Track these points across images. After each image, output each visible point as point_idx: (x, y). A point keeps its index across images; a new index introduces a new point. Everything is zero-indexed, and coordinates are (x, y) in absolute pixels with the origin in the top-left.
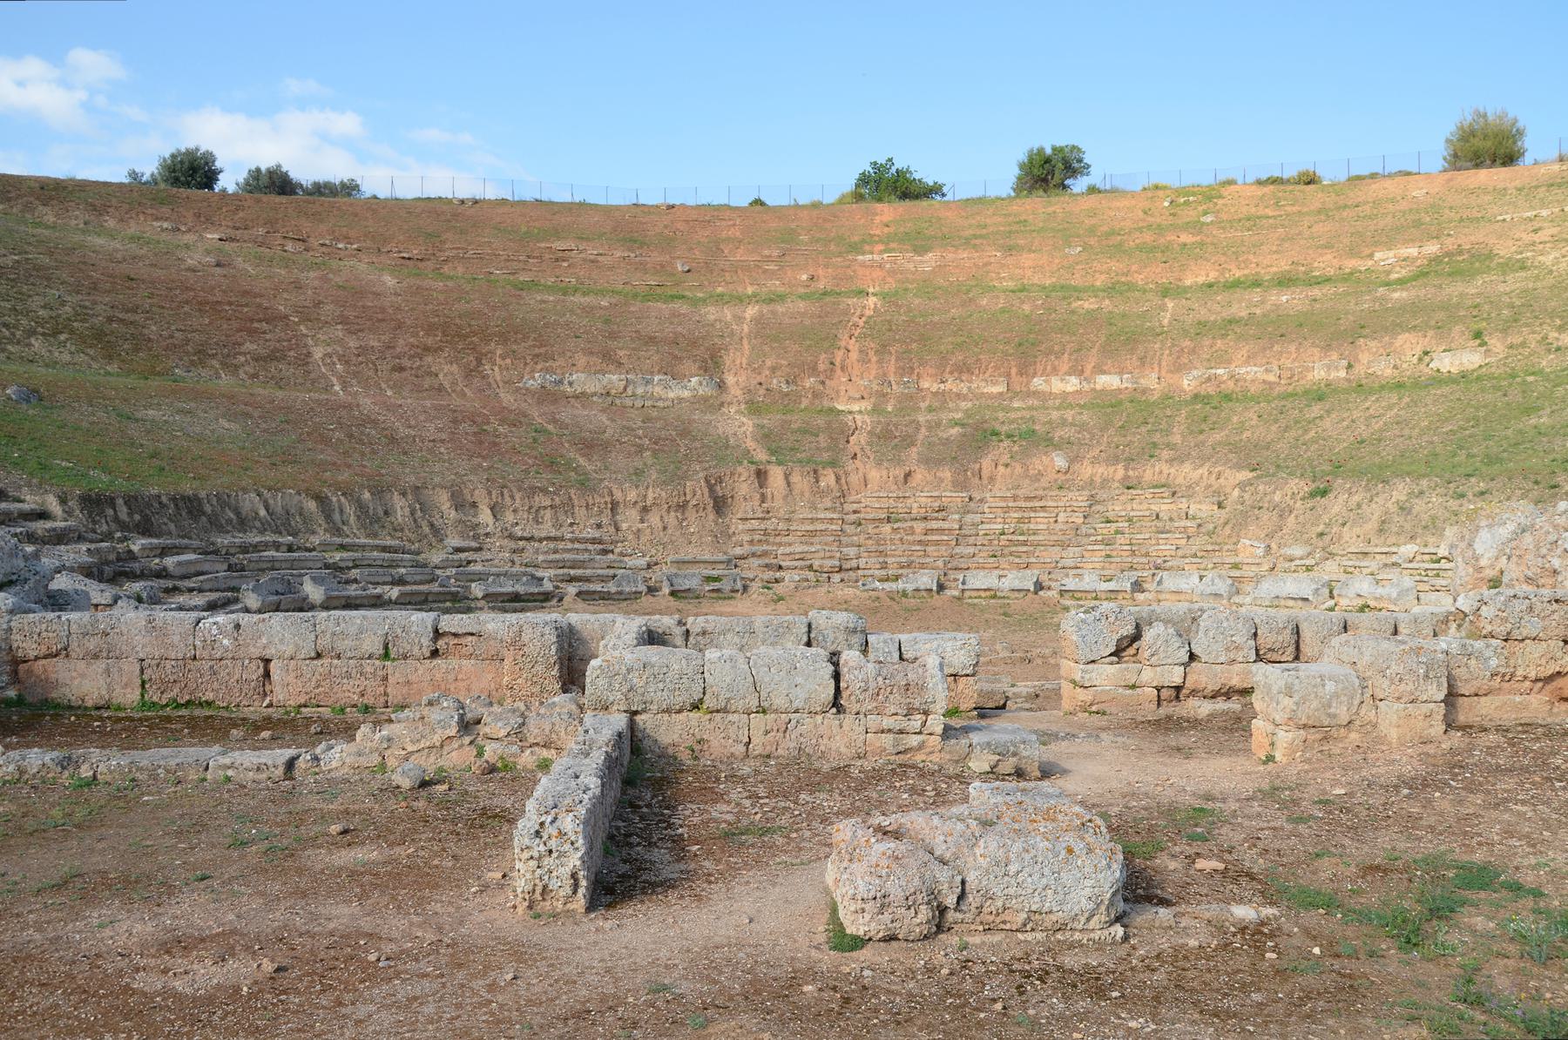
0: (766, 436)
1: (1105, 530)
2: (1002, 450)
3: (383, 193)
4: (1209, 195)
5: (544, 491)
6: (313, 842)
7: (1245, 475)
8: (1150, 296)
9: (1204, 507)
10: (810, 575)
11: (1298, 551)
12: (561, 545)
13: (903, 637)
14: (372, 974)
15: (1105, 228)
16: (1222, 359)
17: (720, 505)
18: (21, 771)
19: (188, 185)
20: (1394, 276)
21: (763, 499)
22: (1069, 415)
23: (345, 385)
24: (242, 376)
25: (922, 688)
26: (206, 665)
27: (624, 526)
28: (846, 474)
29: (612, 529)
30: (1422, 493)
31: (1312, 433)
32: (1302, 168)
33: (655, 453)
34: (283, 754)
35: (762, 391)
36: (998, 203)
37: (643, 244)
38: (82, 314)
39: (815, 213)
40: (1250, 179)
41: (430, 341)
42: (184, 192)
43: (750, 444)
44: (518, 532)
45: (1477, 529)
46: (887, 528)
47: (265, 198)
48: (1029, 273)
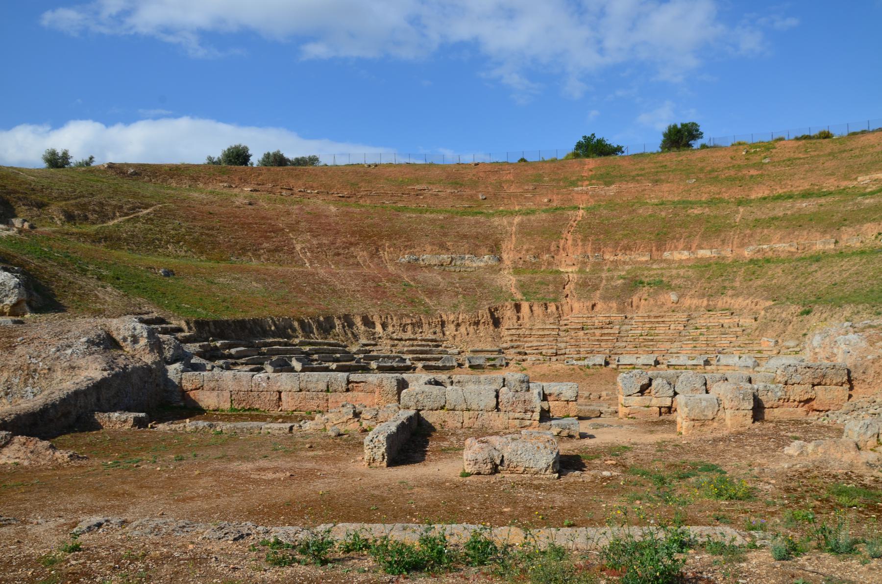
0: (522, 286)
1: (694, 333)
2: (644, 292)
3: (330, 163)
4: (768, 147)
5: (408, 316)
6: (301, 450)
7: (770, 303)
8: (731, 205)
9: (747, 321)
10: (541, 357)
11: (792, 343)
12: (415, 343)
13: (545, 384)
14: (319, 477)
15: (709, 168)
16: (767, 240)
17: (497, 323)
18: (197, 428)
19: (235, 163)
20: (869, 190)
21: (519, 318)
22: (682, 272)
23: (311, 263)
24: (262, 260)
25: (531, 402)
26: (256, 394)
27: (447, 333)
28: (562, 305)
29: (441, 335)
30: (858, 312)
31: (810, 280)
32: (822, 129)
33: (464, 295)
34: (288, 425)
35: (521, 262)
36: (652, 156)
37: (461, 185)
38: (190, 231)
39: (552, 165)
40: (792, 137)
41: (353, 240)
42: (234, 167)
43: (514, 290)
44: (395, 336)
45: (815, 335)
46: (581, 333)
47: (272, 168)
48: (666, 194)
